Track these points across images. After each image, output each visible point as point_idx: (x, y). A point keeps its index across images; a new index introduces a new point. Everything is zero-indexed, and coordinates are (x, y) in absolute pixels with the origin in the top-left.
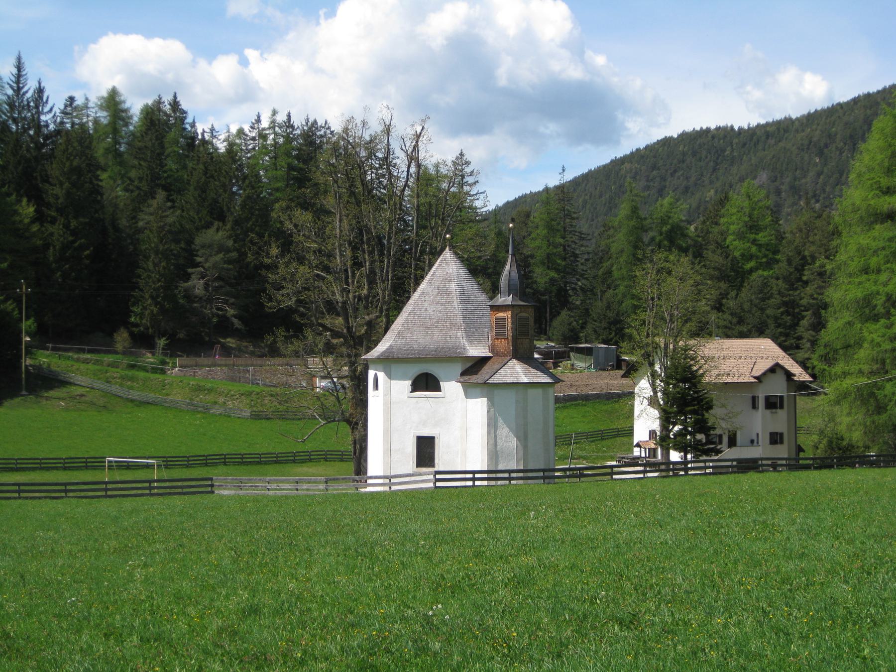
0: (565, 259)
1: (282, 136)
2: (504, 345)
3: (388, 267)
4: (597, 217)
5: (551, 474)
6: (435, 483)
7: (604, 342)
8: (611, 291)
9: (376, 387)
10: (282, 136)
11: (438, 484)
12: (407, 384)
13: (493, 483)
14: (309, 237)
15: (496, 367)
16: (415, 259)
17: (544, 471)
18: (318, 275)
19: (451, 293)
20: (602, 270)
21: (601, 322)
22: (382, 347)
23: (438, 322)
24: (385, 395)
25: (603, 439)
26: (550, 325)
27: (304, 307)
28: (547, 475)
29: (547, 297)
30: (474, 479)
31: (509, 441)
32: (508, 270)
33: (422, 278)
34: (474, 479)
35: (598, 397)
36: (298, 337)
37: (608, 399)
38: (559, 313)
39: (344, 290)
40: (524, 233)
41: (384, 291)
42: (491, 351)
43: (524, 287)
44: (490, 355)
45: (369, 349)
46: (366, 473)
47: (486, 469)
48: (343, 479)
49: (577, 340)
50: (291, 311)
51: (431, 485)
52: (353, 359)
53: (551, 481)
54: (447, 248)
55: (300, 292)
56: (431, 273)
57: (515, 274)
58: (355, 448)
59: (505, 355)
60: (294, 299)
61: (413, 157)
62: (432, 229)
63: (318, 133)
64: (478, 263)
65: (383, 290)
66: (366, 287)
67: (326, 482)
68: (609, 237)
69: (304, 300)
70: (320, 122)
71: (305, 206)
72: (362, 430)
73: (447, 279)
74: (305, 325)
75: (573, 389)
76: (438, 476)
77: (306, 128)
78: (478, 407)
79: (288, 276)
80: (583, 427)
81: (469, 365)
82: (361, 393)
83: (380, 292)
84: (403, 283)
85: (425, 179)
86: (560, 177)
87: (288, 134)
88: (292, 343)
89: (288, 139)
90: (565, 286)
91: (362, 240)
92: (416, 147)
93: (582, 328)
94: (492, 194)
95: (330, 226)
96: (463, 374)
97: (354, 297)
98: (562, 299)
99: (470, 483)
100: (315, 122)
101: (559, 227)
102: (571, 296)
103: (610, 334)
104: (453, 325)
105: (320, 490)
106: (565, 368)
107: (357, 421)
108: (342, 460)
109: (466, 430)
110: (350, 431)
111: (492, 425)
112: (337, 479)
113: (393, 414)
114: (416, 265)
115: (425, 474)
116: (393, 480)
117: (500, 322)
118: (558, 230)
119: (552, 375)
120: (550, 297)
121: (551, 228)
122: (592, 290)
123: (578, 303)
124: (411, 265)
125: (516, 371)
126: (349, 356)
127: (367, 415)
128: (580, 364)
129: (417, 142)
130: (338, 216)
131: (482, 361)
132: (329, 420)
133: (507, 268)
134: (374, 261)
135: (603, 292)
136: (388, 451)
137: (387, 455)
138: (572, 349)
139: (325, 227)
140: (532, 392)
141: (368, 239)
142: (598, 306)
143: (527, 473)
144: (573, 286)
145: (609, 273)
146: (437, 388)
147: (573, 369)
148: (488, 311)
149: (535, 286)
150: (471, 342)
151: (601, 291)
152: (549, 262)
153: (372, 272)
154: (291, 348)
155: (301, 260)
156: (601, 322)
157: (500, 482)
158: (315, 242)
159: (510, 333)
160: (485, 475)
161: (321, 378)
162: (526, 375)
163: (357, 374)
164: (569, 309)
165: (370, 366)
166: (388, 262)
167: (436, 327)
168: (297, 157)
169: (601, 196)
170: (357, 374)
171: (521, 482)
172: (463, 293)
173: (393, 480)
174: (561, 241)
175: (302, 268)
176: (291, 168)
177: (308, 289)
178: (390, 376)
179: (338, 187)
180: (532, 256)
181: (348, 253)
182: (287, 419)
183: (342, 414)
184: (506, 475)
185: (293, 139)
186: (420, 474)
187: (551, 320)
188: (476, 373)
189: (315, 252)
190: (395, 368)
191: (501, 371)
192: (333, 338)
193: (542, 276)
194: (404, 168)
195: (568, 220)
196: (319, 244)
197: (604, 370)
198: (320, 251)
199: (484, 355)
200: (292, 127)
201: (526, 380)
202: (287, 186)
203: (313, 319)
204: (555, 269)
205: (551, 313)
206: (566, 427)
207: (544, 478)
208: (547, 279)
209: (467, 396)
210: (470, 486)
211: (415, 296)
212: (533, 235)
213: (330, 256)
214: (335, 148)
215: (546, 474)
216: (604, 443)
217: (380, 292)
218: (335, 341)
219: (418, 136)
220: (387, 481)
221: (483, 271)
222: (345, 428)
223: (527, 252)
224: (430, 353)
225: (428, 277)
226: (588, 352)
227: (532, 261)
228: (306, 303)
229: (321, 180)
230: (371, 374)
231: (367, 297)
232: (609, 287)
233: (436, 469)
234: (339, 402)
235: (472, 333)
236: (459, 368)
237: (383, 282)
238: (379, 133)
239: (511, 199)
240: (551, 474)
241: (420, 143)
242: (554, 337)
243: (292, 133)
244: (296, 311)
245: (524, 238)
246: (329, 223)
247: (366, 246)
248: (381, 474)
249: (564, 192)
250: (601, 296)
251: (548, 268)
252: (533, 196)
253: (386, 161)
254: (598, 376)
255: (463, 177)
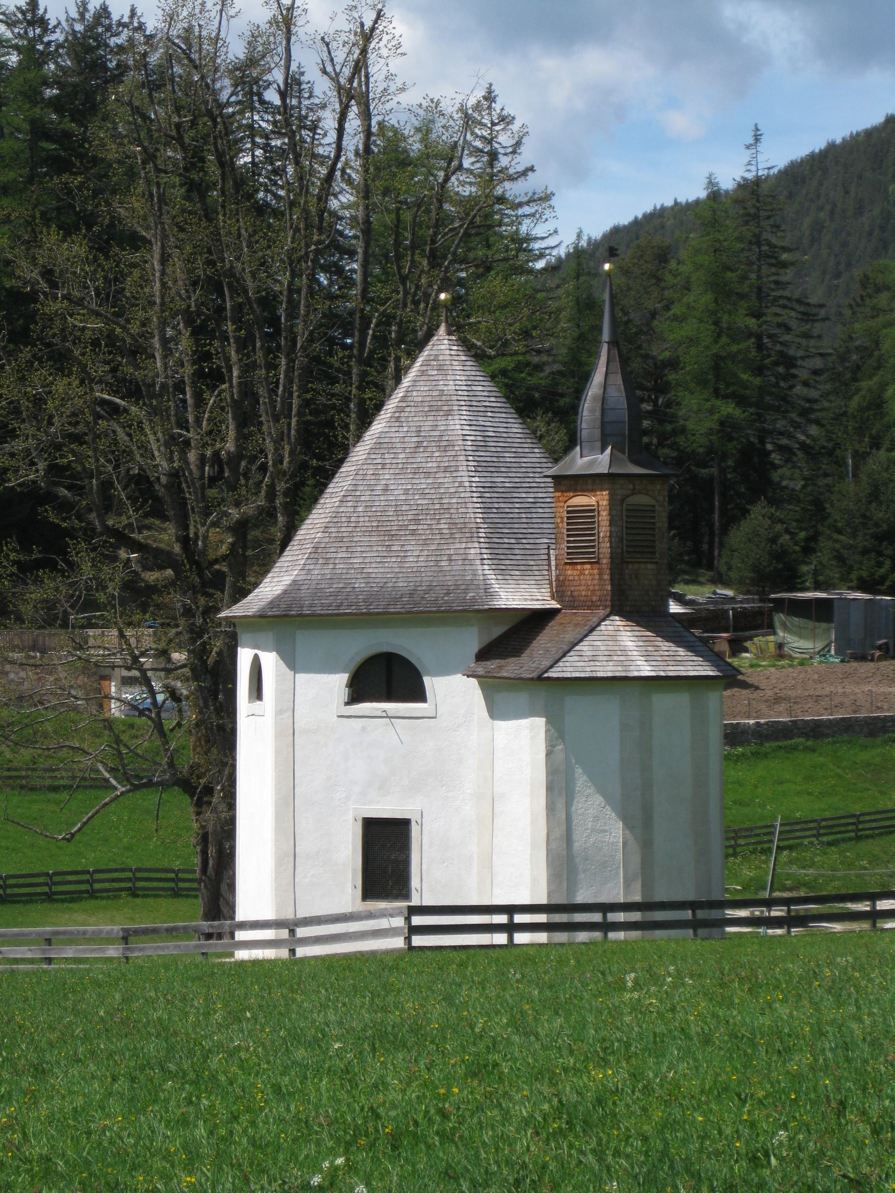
0: (759, 370)
1: (16, 47)
2: (591, 579)
3: (289, 380)
4: (849, 265)
5: (715, 914)
6: (408, 939)
7: (863, 586)
8: (882, 454)
9: (257, 691)
10: (16, 47)
11: (418, 941)
12: (339, 682)
13: (561, 937)
14: (80, 302)
15: (570, 636)
16: (361, 361)
17: (693, 905)
18: (103, 402)
19: (451, 444)
20: (856, 398)
21: (854, 535)
22: (270, 588)
23: (417, 521)
24: (279, 712)
25: (858, 838)
26: (722, 545)
27: (69, 488)
28: (703, 915)
29: (715, 471)
30: (511, 928)
31: (604, 829)
32: (601, 381)
33: (379, 407)
34: (511, 928)
35: (847, 727)
36: (53, 566)
37: (872, 734)
38: (745, 512)
39: (171, 440)
40: (651, 304)
41: (278, 441)
42: (557, 594)
43: (642, 432)
44: (555, 605)
45: (241, 593)
46: (233, 918)
47: (543, 900)
48: (170, 930)
49: (792, 582)
50: (34, 496)
51: (398, 943)
52: (199, 621)
53: (715, 931)
54: (442, 330)
55: (59, 447)
56: (399, 393)
57: (618, 394)
58: (204, 853)
59: (592, 606)
60: (42, 466)
61: (354, 92)
62: (403, 279)
63: (113, 41)
64: (533, 381)
65: (277, 444)
66: (232, 434)
67: (125, 939)
68: (877, 312)
69: (68, 467)
70: (119, 11)
71: (72, 220)
72: (222, 807)
73: (439, 407)
74: (70, 533)
75: (782, 707)
76: (417, 920)
77: (79, 27)
78: (523, 742)
79: (24, 403)
80: (804, 807)
81: (498, 631)
82: (218, 711)
83: (269, 445)
84: (330, 424)
85: (389, 160)
86: (746, 155)
87: (33, 42)
88: (38, 581)
89: (34, 57)
90: (762, 441)
91: (220, 309)
92: (360, 66)
93: (808, 550)
94: (576, 212)
95: (136, 273)
96: (483, 655)
97: (202, 459)
98: (753, 475)
99: (501, 938)
100: (104, 12)
101: (745, 288)
102: (775, 467)
103: (880, 565)
104: (460, 529)
105: (110, 960)
106: (762, 653)
107: (207, 783)
108: (176, 893)
109: (489, 801)
110: (192, 810)
111: (559, 789)
112: (155, 931)
113: (302, 763)
114: (363, 375)
115: (383, 914)
116: (301, 932)
117: (579, 520)
118: (742, 296)
119: (716, 659)
120: (723, 471)
121: (723, 292)
122: (831, 453)
123: (799, 485)
124: (349, 373)
125: (622, 648)
126: (188, 612)
127: (234, 767)
128: (799, 644)
129: (364, 51)
130: (157, 249)
131: (533, 622)
132: (139, 783)
133: (598, 378)
134: (254, 366)
135: (860, 457)
136: (289, 858)
137: (284, 869)
138: (779, 605)
139: (124, 275)
140: (662, 701)
141: (238, 308)
142: (847, 494)
143: (651, 914)
144: (784, 441)
145: (877, 405)
146: (417, 694)
147: (781, 656)
148: (547, 492)
149: (681, 440)
150: (502, 571)
151: (856, 454)
152: (718, 378)
153: (247, 390)
154: (35, 594)
155: (60, 361)
156: (854, 535)
157: (582, 936)
158: (98, 314)
159: (605, 548)
160: (542, 918)
161: (123, 681)
162: (648, 657)
163: (211, 661)
164: (771, 502)
165: (242, 637)
166: (290, 369)
167: (413, 533)
168: (56, 104)
169: (859, 210)
170: (211, 661)
171: (635, 934)
172: (482, 445)
173: (301, 932)
174: (752, 322)
175: (60, 385)
176: (39, 131)
177: (77, 439)
178: (292, 662)
179: (158, 170)
180: (673, 364)
181: (185, 343)
182: (33, 789)
183: (171, 764)
184: (597, 917)
185: (45, 56)
186: (370, 916)
187: (725, 530)
188: (517, 652)
189: (96, 343)
190: (306, 640)
191: (584, 647)
192: (146, 568)
193: (699, 415)
194: (329, 121)
195: (765, 270)
196: (107, 321)
197: (863, 658)
198: (111, 338)
199: (537, 605)
200: (42, 22)
201: (646, 670)
202: (30, 180)
203: (93, 516)
204: (733, 396)
205: (723, 514)
206: (763, 806)
207: (695, 925)
208: (710, 423)
209: (495, 711)
210: (500, 946)
211: (360, 453)
212: (676, 310)
213: (138, 351)
214: (156, 82)
215: (701, 914)
216: (864, 846)
217: (269, 445)
218: (151, 577)
219: (367, 36)
220: (284, 934)
221: (539, 399)
222: (179, 805)
223: (661, 352)
224: (396, 600)
225: (391, 405)
226: (821, 612)
227: (672, 377)
228: (74, 477)
229: (112, 152)
230: (245, 657)
231: (235, 459)
232: (876, 444)
233: (415, 901)
234: (162, 733)
235: (506, 553)
236: (471, 640)
237: (276, 419)
238: (264, 27)
239: (625, 219)
240: (715, 914)
241: (372, 57)
242: (733, 575)
243: (40, 37)
244: (49, 498)
245: (653, 315)
246: (134, 265)
247: (230, 327)
248: (269, 915)
249: (756, 201)
250: (856, 467)
251: (717, 393)
252: (680, 211)
253: (292, 121)
254: (847, 676)
255: (493, 156)
